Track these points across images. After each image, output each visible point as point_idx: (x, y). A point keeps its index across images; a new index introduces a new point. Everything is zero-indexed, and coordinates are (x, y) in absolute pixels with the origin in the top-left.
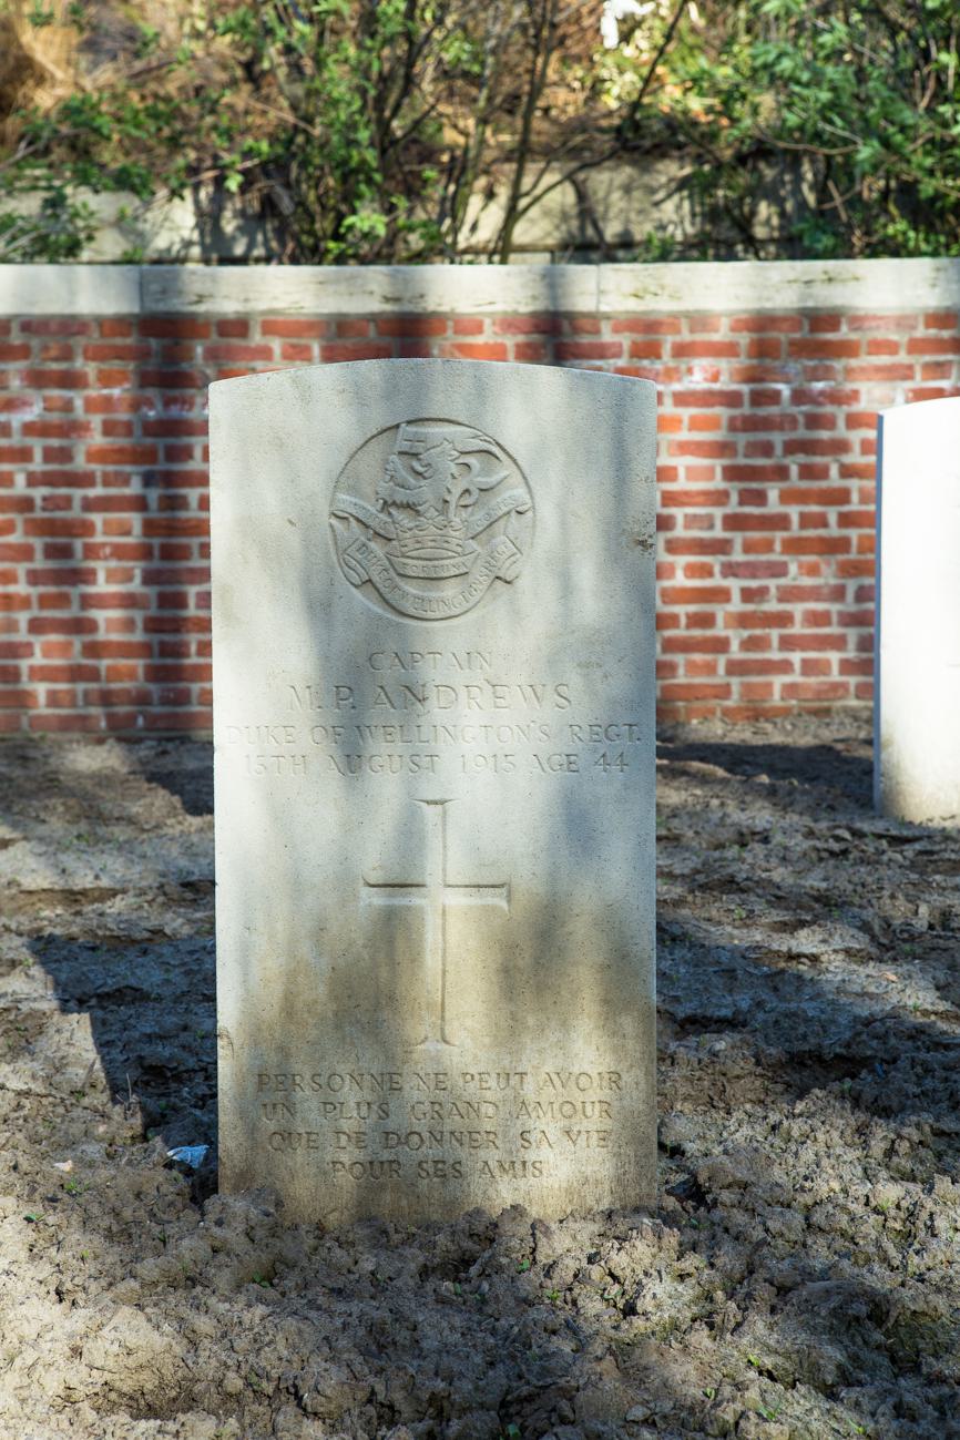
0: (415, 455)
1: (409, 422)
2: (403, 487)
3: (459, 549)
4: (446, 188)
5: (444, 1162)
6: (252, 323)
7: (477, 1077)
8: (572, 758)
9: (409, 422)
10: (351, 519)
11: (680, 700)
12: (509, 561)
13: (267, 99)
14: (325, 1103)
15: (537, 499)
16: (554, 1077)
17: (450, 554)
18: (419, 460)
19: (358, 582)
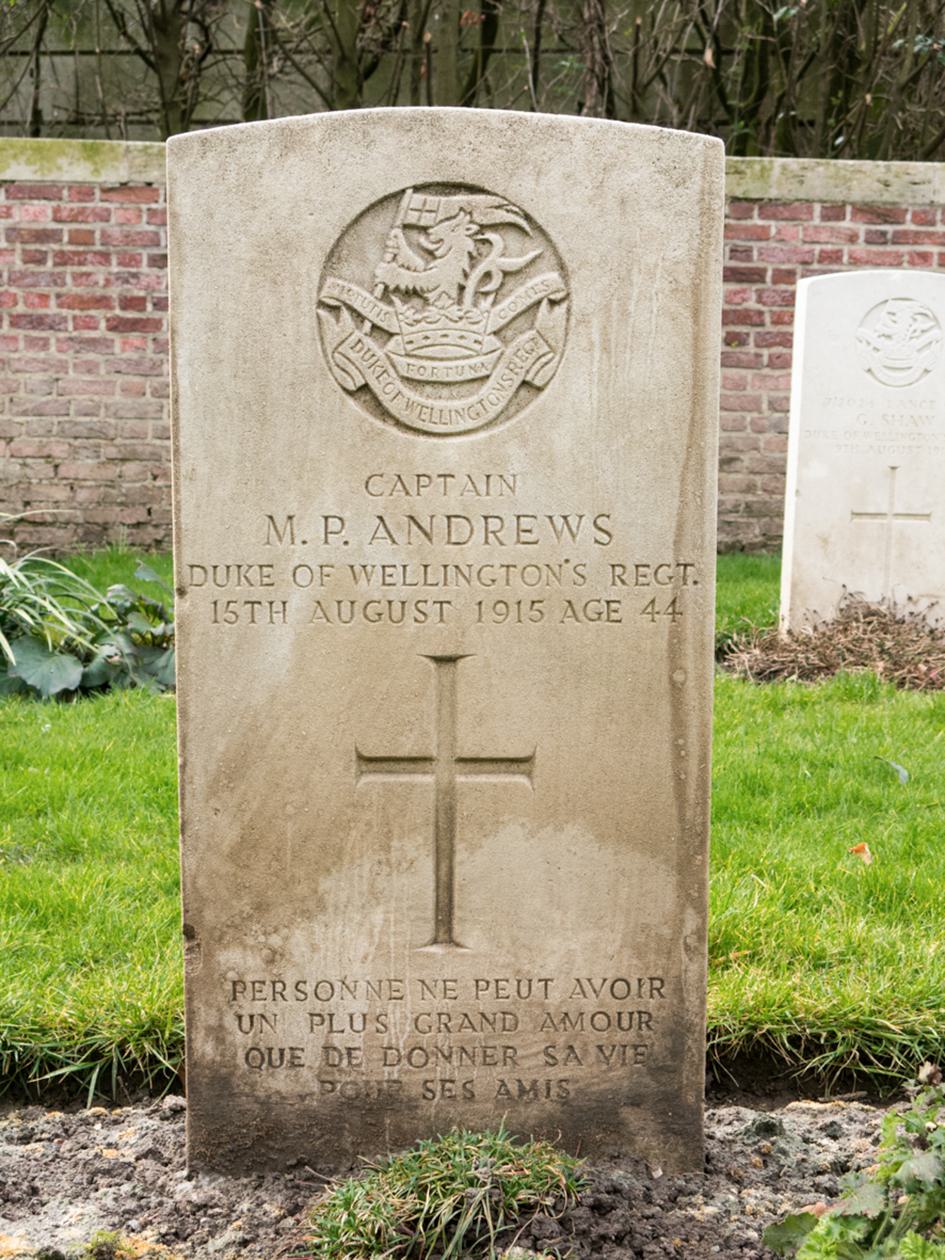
0: (424, 229)
1: (417, 189)
2: (408, 268)
3: (477, 347)
4: (96, 115)
5: (452, 1081)
6: (7, 226)
7: (493, 985)
8: (614, 606)
9: (417, 189)
10: (343, 308)
11: (354, 44)
12: (538, 365)
13: (586, 960)
14: (312, 1015)
15: (573, 284)
16: (585, 984)
17: (468, 352)
18: (428, 235)
19: (352, 387)
